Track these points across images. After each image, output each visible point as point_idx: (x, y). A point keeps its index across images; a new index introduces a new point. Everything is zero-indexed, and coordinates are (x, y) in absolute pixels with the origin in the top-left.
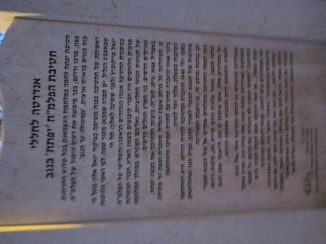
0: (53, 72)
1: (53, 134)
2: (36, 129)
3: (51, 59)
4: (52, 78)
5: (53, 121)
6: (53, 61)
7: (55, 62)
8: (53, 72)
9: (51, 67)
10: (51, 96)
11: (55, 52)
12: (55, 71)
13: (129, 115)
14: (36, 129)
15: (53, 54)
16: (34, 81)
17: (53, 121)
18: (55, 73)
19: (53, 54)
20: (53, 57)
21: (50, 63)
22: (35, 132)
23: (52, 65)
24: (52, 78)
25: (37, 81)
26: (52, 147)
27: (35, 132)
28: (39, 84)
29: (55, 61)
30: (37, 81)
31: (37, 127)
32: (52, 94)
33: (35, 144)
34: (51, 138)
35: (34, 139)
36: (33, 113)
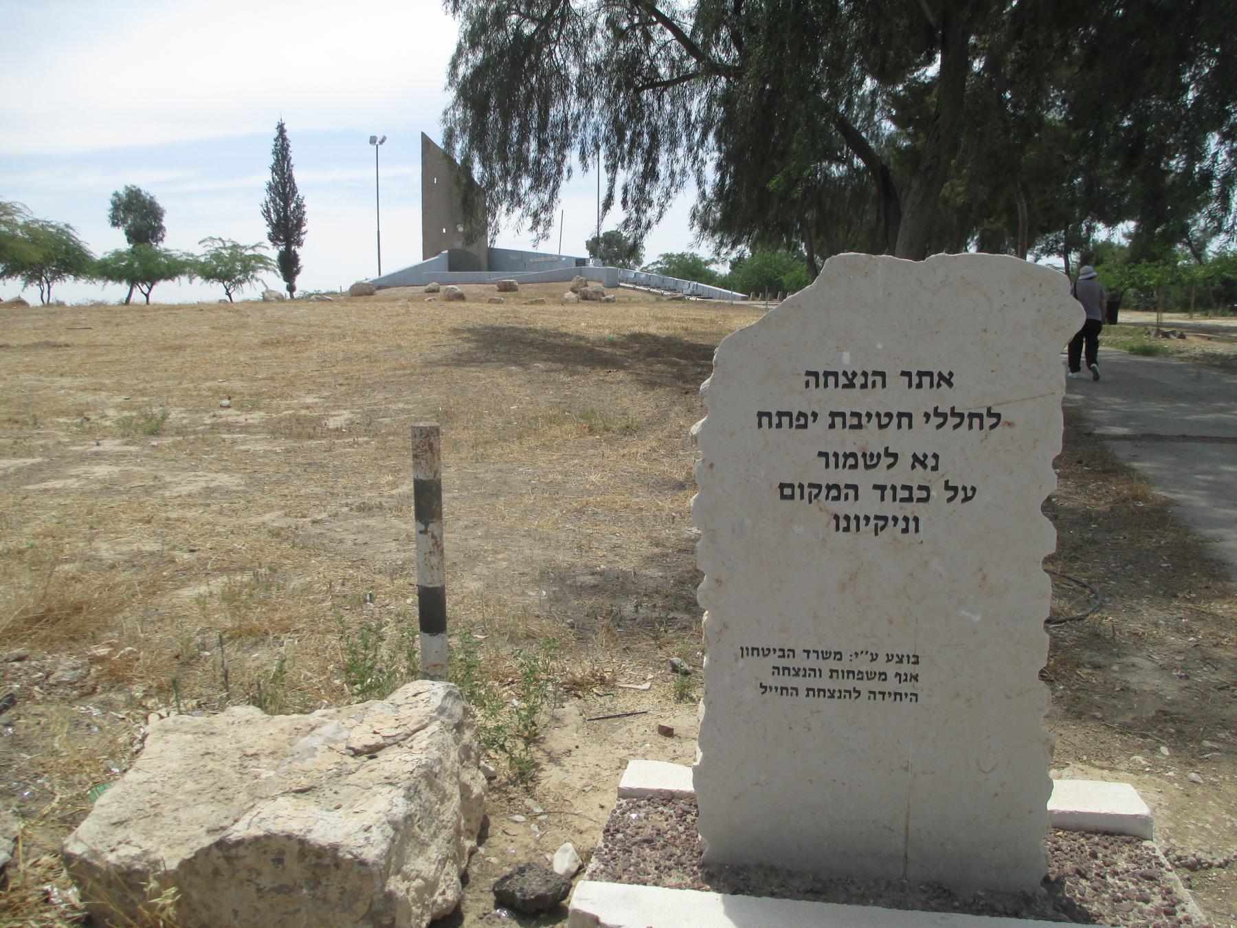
0: (855, 421)
1: (805, 426)
2: (976, 421)
3: (889, 415)
4: (838, 420)
5: (760, 425)
6: (885, 420)
7: (881, 427)
8: (855, 421)
9: (869, 415)
10: (798, 419)
11: (910, 426)
12: (859, 426)
13: (871, 461)
14: (976, 421)
15: (905, 421)
16: (946, 374)
17: (760, 425)
18: (852, 427)
19: (905, 421)
20: (895, 420)
21: (878, 415)
22: (966, 420)
23: (874, 420)
24: (838, 420)
25: (947, 380)
26: (770, 425)
27: (966, 420)
28: (939, 385)
29: (886, 426)
30: (947, 380)
31: (981, 427)
32: (802, 421)
33: (936, 421)
34: (795, 423)
35: (949, 417)
36: (808, 373)
